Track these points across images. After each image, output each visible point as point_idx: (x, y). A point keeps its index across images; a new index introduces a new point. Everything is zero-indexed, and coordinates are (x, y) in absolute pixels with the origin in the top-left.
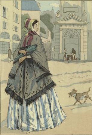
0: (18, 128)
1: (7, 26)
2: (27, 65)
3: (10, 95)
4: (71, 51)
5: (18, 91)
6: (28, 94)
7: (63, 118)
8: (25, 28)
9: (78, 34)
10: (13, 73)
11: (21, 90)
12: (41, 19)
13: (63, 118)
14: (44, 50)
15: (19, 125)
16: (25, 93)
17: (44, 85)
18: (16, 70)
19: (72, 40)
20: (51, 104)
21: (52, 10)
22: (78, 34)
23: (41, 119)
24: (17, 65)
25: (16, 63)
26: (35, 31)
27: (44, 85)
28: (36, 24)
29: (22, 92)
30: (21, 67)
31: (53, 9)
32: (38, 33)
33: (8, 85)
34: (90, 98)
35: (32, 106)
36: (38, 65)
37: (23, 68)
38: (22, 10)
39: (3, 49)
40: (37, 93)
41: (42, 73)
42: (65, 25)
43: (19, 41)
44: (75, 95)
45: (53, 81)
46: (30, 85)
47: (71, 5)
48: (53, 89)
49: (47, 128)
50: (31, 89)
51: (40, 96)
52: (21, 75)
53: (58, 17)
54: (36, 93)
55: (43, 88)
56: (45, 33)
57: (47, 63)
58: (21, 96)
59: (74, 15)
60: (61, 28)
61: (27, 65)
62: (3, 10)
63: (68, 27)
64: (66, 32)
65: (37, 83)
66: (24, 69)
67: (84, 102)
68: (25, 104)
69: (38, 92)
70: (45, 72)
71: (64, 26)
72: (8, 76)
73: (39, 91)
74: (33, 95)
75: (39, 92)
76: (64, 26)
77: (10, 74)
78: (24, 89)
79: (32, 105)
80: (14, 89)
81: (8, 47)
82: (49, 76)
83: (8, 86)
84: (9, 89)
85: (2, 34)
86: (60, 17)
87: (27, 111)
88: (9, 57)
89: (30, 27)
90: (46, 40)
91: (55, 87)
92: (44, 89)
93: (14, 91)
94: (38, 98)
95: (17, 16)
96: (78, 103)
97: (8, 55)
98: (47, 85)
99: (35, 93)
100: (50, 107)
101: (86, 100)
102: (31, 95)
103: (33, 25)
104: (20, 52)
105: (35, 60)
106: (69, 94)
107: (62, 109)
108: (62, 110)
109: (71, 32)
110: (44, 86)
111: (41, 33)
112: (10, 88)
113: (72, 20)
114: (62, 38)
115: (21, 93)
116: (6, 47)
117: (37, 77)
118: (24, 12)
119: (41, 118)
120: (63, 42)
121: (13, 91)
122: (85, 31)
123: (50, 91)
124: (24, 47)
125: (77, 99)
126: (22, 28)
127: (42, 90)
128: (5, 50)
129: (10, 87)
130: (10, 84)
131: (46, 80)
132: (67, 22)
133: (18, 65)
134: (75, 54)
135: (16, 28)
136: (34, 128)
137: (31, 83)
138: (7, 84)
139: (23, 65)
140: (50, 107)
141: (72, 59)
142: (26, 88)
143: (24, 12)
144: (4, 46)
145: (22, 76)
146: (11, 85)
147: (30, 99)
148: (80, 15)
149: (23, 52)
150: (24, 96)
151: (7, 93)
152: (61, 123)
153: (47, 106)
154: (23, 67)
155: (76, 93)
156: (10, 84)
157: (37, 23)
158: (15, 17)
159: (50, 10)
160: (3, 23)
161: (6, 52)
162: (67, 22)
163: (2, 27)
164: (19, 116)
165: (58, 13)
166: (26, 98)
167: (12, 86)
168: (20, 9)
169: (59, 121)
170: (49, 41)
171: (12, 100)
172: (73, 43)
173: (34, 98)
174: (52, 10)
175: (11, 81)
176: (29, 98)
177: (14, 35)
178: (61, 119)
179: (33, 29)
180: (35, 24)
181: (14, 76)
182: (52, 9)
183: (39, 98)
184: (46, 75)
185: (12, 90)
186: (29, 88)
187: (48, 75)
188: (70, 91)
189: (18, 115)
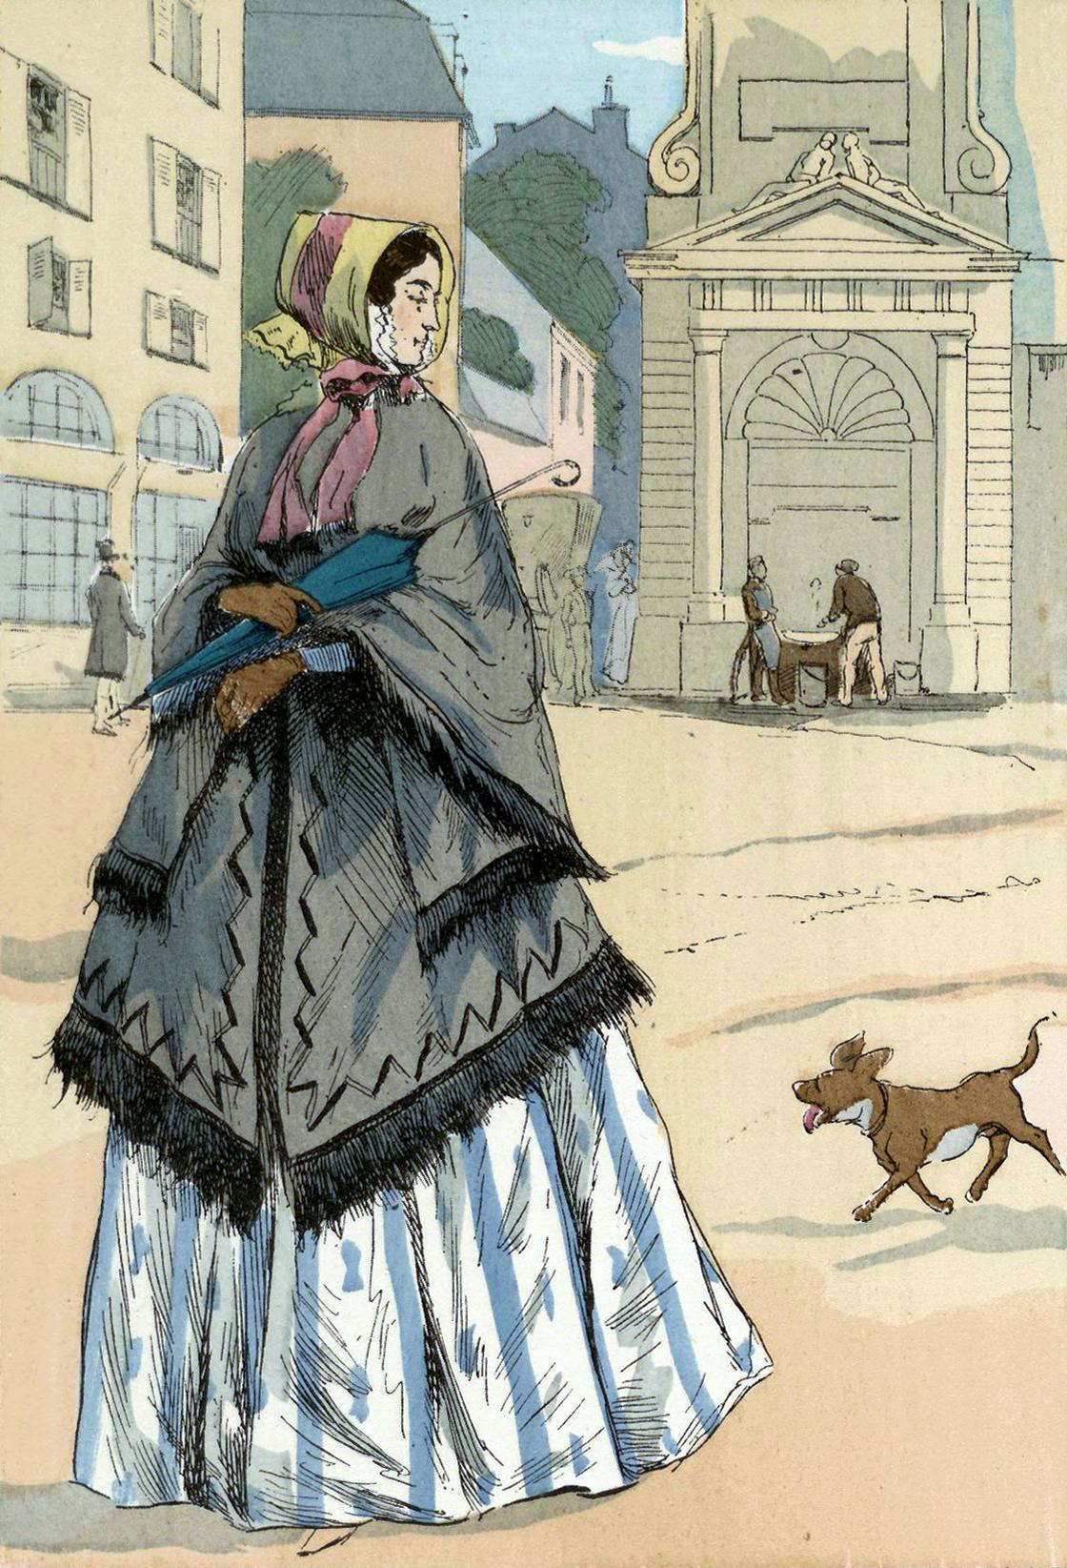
0: (199, 1492)
1: (76, 299)
2: (309, 752)
3: (113, 1108)
4: (826, 596)
5: (202, 1061)
6: (324, 1091)
7: (720, 1380)
8: (288, 325)
9: (914, 400)
10: (151, 852)
11: (240, 1042)
12: (474, 217)
13: (720, 1380)
14: (504, 589)
15: (212, 1451)
16: (281, 1078)
17: (508, 993)
18: (181, 814)
19: (837, 465)
20: (594, 1208)
21: (610, 108)
22: (914, 400)
23: (468, 1389)
24: (193, 757)
25: (179, 736)
26: (409, 355)
27: (508, 993)
28: (416, 273)
29: (248, 1073)
30: (238, 775)
31: (620, 98)
32: (442, 377)
33: (84, 986)
34: (1040, 1141)
35: (359, 1226)
36: (438, 760)
37: (264, 788)
38: (246, 111)
39: (37, 569)
40: (424, 1080)
41: (489, 849)
42: (758, 283)
43: (220, 479)
44: (864, 1109)
45: (607, 943)
46: (342, 1006)
47: (818, 52)
48: (612, 1034)
49: (538, 1488)
50: (360, 1037)
51: (467, 1122)
52: (233, 864)
53: (670, 187)
54: (414, 1085)
55: (499, 1028)
56: (522, 380)
57: (545, 731)
58: (241, 1116)
59: (861, 172)
60: (707, 319)
61: (309, 752)
62: (34, 109)
63: (789, 309)
64: (764, 369)
65: (426, 963)
66: (280, 806)
67: (978, 1189)
68: (286, 1219)
69: (430, 1071)
70: (518, 842)
71: (737, 297)
72: (81, 890)
73: (449, 1061)
74: (385, 1099)
75: (450, 1072)
76: (737, 297)
77: (116, 863)
78: (274, 1036)
79: (366, 1219)
80: (155, 1033)
81: (87, 547)
82: (566, 883)
83: (91, 1005)
84: (98, 1037)
85: (20, 392)
86: (694, 192)
87: (304, 1300)
88: (101, 666)
89: (343, 313)
90: (528, 460)
91: (637, 1008)
92: (513, 1026)
93: (160, 1059)
94: (438, 1143)
95: (189, 178)
96: (904, 1197)
97: (86, 634)
98: (539, 986)
99: (399, 1086)
100: (581, 1244)
101: (994, 1164)
102: (352, 1111)
103: (381, 289)
104: (229, 602)
105: (405, 693)
106: (808, 1091)
107: (722, 1277)
108: (717, 1287)
109: (825, 368)
110: (511, 1007)
111: (477, 380)
112: (102, 1026)
113: (830, 223)
114: (724, 438)
115: (241, 1083)
116: (64, 545)
117: (428, 893)
118: (280, 136)
119: (469, 1367)
120: (550, 742)
121: (143, 1062)
122: (992, 363)
123: (574, 1067)
124: (272, 550)
125: (887, 1160)
126: (252, 320)
127: (490, 1045)
128: (154, 559)
129: (109, 1017)
130: (112, 980)
131: (525, 936)
132: (767, 258)
133: (209, 763)
134: (866, 630)
135: (183, 321)
136: (721, 695)
137: (352, 970)
138: (76, 980)
139: (263, 752)
140: (581, 1244)
141: (832, 685)
142: (299, 1024)
143: (280, 136)
144: (38, 535)
145: (305, 845)
146: (120, 992)
147: (345, 1153)
148: (927, 176)
149: (266, 603)
150: (269, 1113)
151: (73, 1087)
152: (700, 1431)
153: (544, 1224)
154: (266, 779)
155: (881, 1087)
156: (112, 980)
157: (428, 269)
158: (167, 196)
159: (580, 105)
160: (34, 273)
161: (63, 605)
162: (767, 258)
163: (16, 308)
164: (215, 1346)
165: (669, 150)
166: (300, 1140)
167: (133, 1004)
168: (231, 95)
169: (678, 1414)
170: (567, 474)
171: (134, 1168)
172: (852, 498)
173: (387, 1137)
174: (610, 108)
175: (123, 934)
176: (337, 1143)
177: (158, 407)
178: (696, 1392)
179: (375, 329)
180: (398, 272)
181: (157, 886)
182: (599, 98)
183: (454, 1137)
184: (527, 872)
185: (138, 1046)
186: (332, 1029)
187: (561, 873)
188: (820, 1063)
189: (205, 1339)
